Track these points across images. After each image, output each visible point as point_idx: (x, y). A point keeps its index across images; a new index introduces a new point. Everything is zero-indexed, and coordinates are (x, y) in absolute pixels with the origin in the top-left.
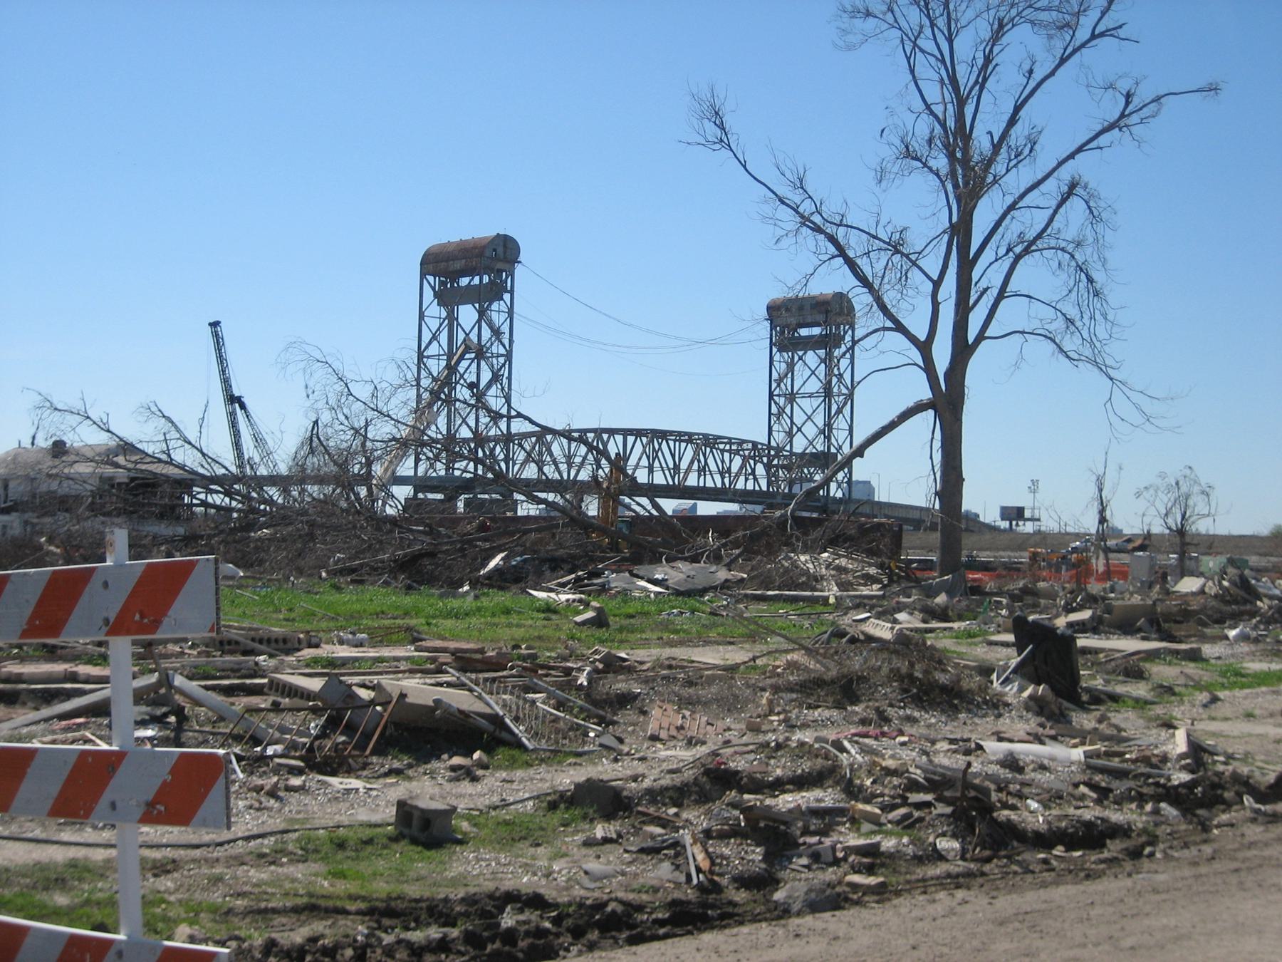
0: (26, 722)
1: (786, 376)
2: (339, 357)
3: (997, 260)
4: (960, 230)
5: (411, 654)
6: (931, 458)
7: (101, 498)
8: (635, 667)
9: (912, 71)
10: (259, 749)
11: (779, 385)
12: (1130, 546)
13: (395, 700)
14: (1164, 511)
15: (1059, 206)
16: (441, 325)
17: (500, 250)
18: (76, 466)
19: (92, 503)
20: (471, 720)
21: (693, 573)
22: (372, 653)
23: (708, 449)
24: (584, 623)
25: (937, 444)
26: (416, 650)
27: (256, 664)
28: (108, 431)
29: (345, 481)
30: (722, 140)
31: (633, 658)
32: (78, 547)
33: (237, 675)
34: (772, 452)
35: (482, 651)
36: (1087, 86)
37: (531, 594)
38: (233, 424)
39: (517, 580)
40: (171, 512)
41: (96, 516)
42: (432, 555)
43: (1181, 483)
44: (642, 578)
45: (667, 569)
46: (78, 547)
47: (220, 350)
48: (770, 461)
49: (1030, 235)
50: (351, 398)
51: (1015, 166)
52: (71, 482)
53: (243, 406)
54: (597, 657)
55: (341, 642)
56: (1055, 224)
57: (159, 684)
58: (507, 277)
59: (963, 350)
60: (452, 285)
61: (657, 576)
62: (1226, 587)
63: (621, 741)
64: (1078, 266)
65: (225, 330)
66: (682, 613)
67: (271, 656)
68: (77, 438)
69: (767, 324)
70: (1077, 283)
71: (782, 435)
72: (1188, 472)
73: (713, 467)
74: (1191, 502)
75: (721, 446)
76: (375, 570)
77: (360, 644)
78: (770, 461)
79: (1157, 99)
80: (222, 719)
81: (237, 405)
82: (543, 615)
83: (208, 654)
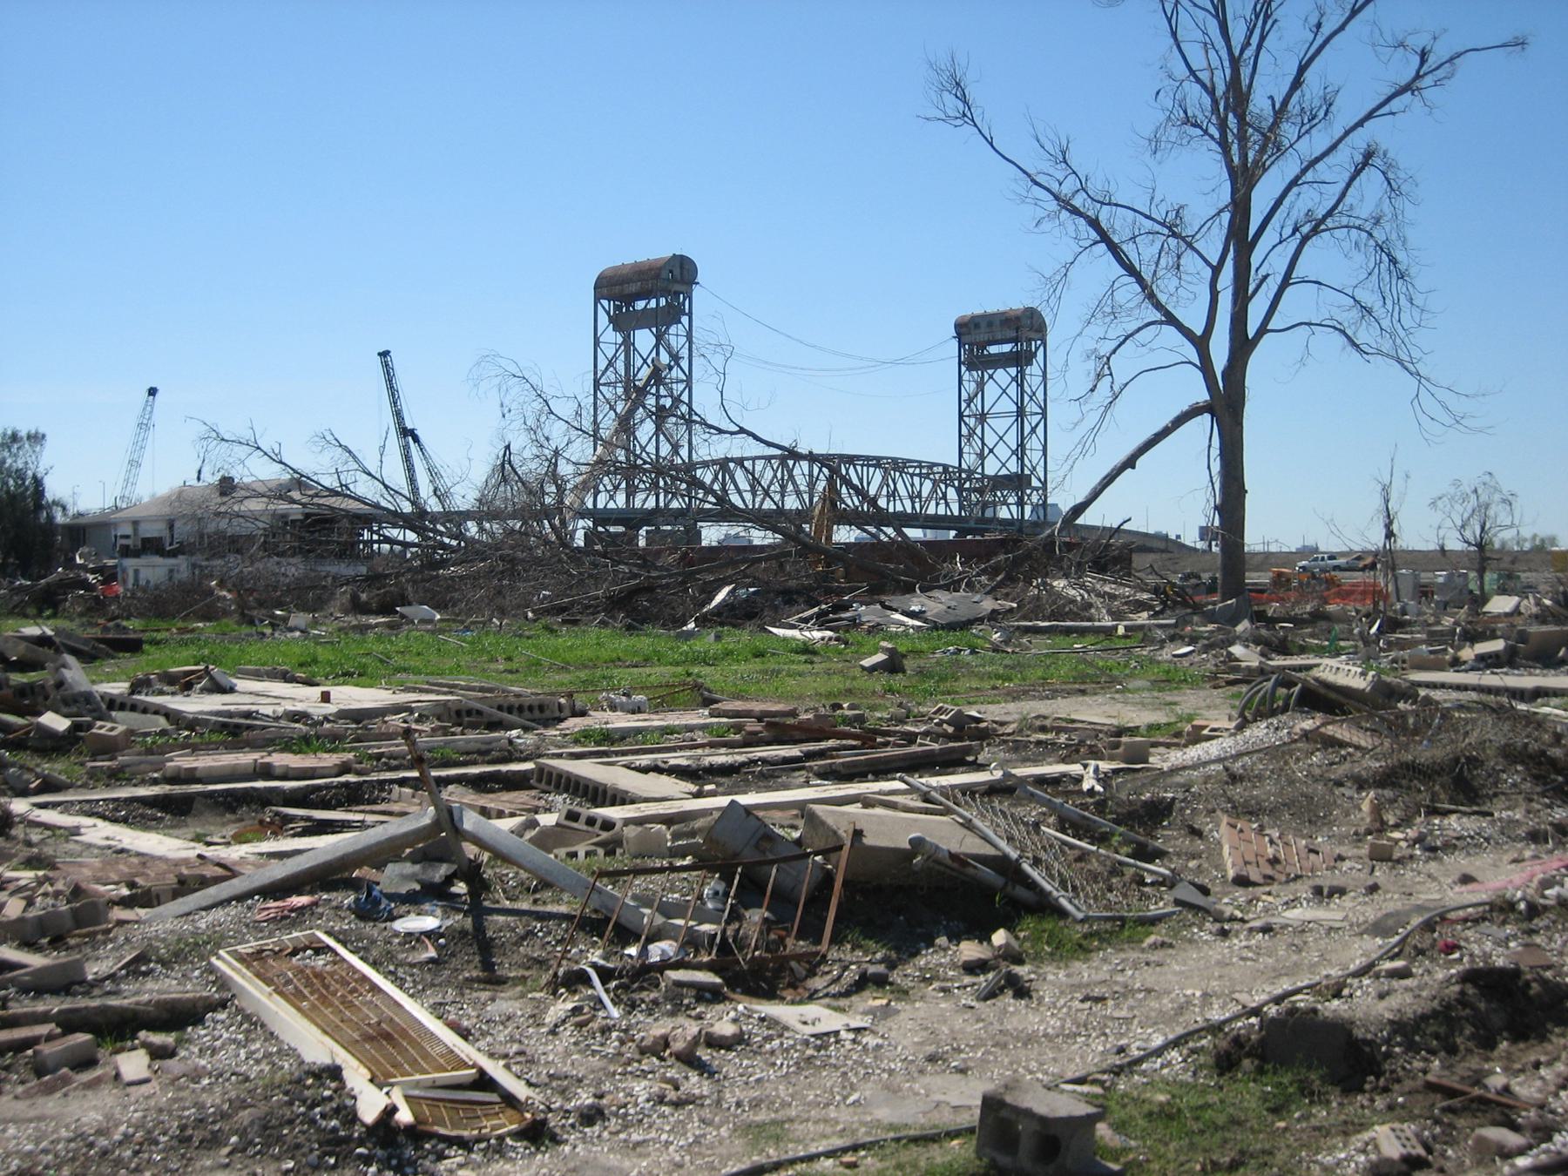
0: (204, 904)
1: (976, 395)
2: (537, 370)
3: (1281, 242)
4: (1240, 207)
6: (1209, 467)
7: (274, 537)
8: (995, 730)
9: (1174, 34)
10: (632, 951)
11: (969, 406)
12: (1361, 564)
13: (848, 843)
14: (1459, 523)
15: (1352, 179)
17: (677, 272)
18: (246, 502)
19: (265, 542)
20: (971, 871)
21: (953, 604)
22: (657, 721)
24: (872, 669)
25: (1215, 452)
26: (711, 715)
27: (510, 742)
28: (281, 462)
29: (534, 512)
30: (964, 115)
31: (989, 717)
32: (251, 591)
33: (487, 758)
34: (964, 476)
35: (793, 713)
36: (1374, 45)
38: (407, 458)
40: (348, 551)
41: (269, 556)
42: (650, 589)
43: (1480, 491)
44: (896, 611)
46: (251, 591)
47: (390, 381)
48: (961, 485)
49: (1320, 214)
51: (1307, 132)
52: (241, 520)
53: (416, 439)
54: (943, 717)
55: (613, 708)
56: (1348, 200)
57: (436, 825)
59: (1242, 346)
60: (627, 309)
61: (913, 608)
62: (1547, 607)
63: (1205, 891)
64: (1377, 245)
65: (396, 360)
67: (526, 729)
68: (246, 472)
69: (955, 343)
70: (1379, 264)
71: (973, 457)
72: (1487, 478)
74: (1491, 513)
75: (911, 470)
76: (591, 609)
77: (637, 710)
78: (961, 485)
79: (1451, 60)
80: (545, 884)
82: (803, 658)
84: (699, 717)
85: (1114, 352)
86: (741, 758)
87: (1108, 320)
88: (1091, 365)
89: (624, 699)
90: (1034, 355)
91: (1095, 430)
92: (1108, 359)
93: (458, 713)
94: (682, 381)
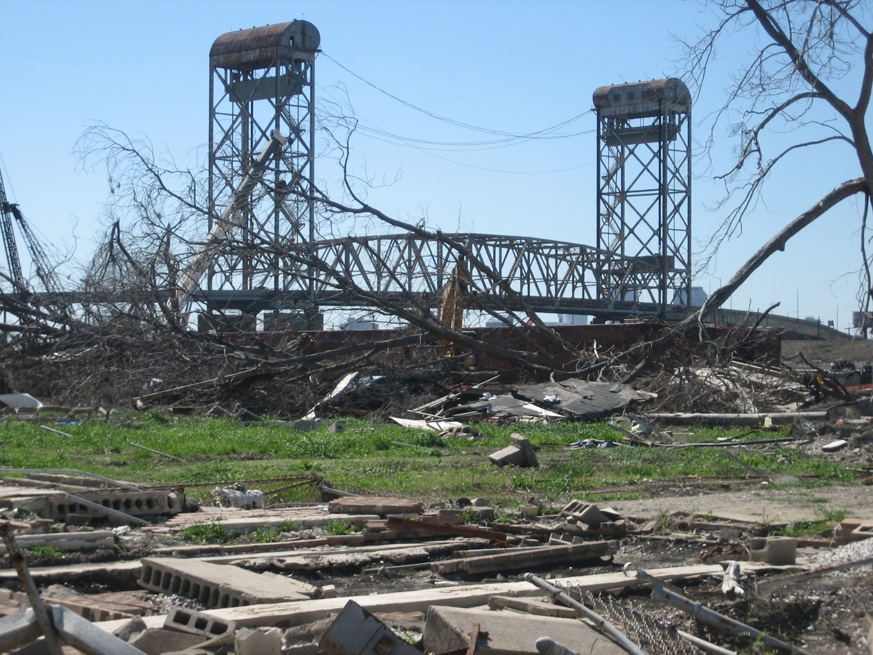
1: (616, 172)
5: (327, 517)
6: (863, 250)
11: (608, 183)
16: (234, 122)
17: (298, 39)
21: (589, 393)
22: (272, 517)
23: (532, 255)
26: (331, 511)
27: (117, 539)
33: (91, 557)
34: (602, 257)
35: (418, 509)
37: (396, 423)
39: (374, 405)
42: (268, 377)
44: (529, 400)
45: (558, 389)
48: (599, 267)
50: (164, 192)
53: (18, 215)
54: (577, 514)
55: (227, 502)
57: (35, 628)
58: (306, 68)
60: (245, 79)
61: (547, 398)
66: (597, 443)
67: (134, 526)
69: (594, 116)
71: (612, 237)
73: (537, 273)
75: (546, 251)
77: (252, 505)
78: (599, 267)
81: (11, 215)
82: (430, 450)
83: (47, 528)
84: (318, 513)
85: (762, 126)
86: (362, 557)
87: (755, 92)
88: (738, 140)
89: (238, 493)
90: (677, 129)
91: (741, 210)
92: (756, 134)
93: (61, 508)
94: (303, 155)
